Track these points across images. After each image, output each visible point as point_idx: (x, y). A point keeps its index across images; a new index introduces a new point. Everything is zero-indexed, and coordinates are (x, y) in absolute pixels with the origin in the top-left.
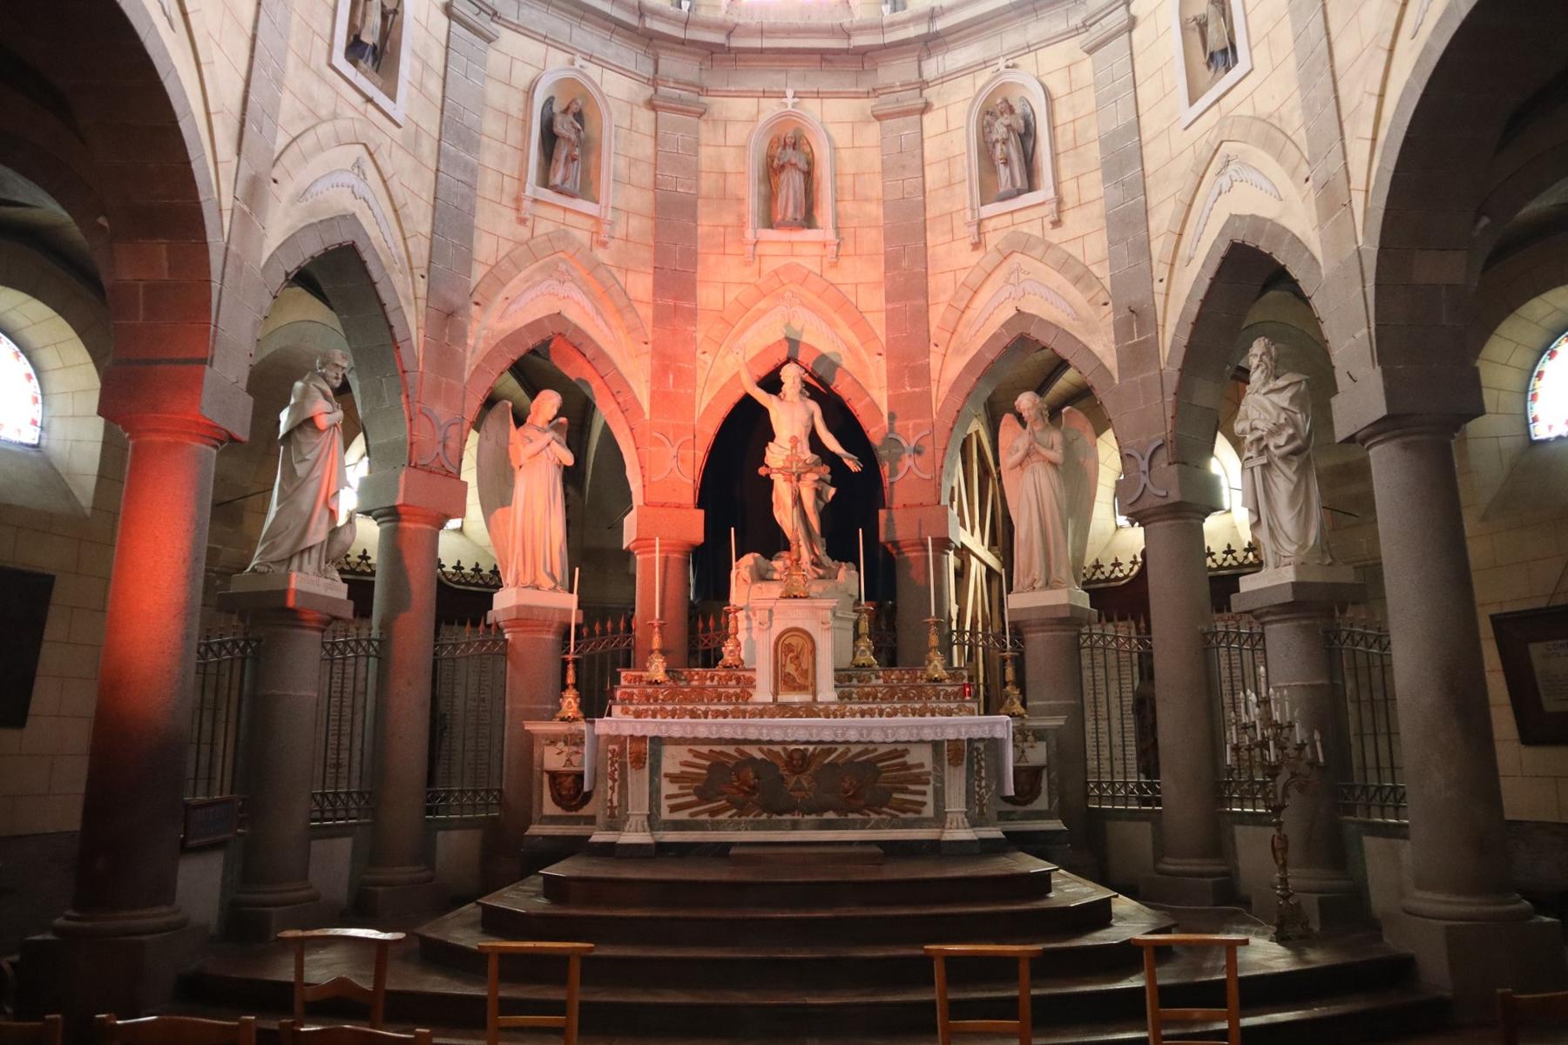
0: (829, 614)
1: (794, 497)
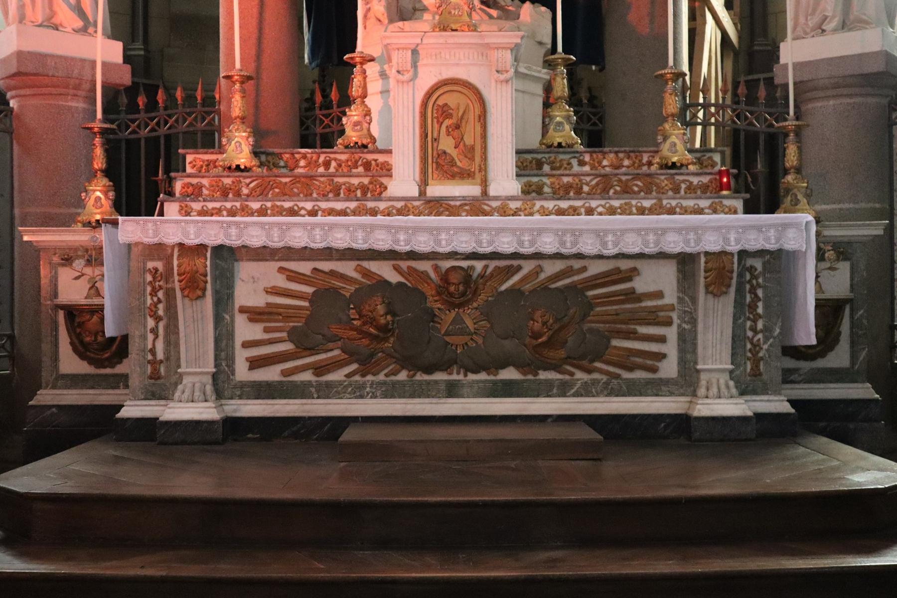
0: (508, 56)
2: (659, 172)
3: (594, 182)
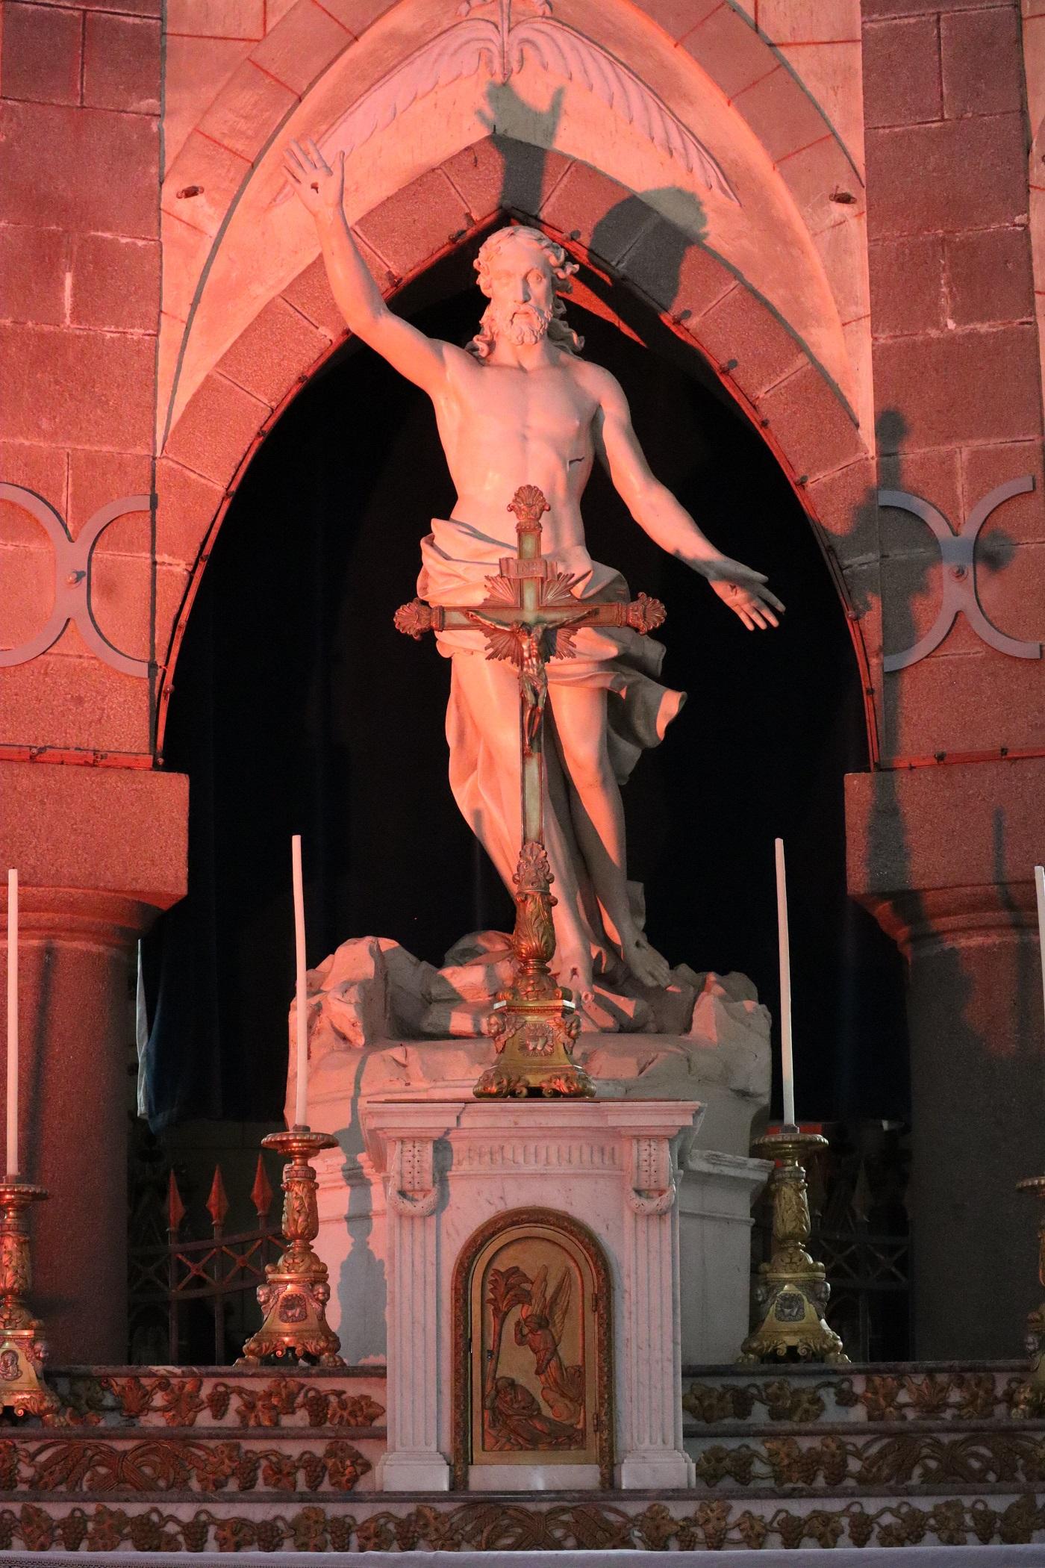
0: (664, 1156)
1: (522, 728)
2: (1028, 1423)
3: (874, 1449)
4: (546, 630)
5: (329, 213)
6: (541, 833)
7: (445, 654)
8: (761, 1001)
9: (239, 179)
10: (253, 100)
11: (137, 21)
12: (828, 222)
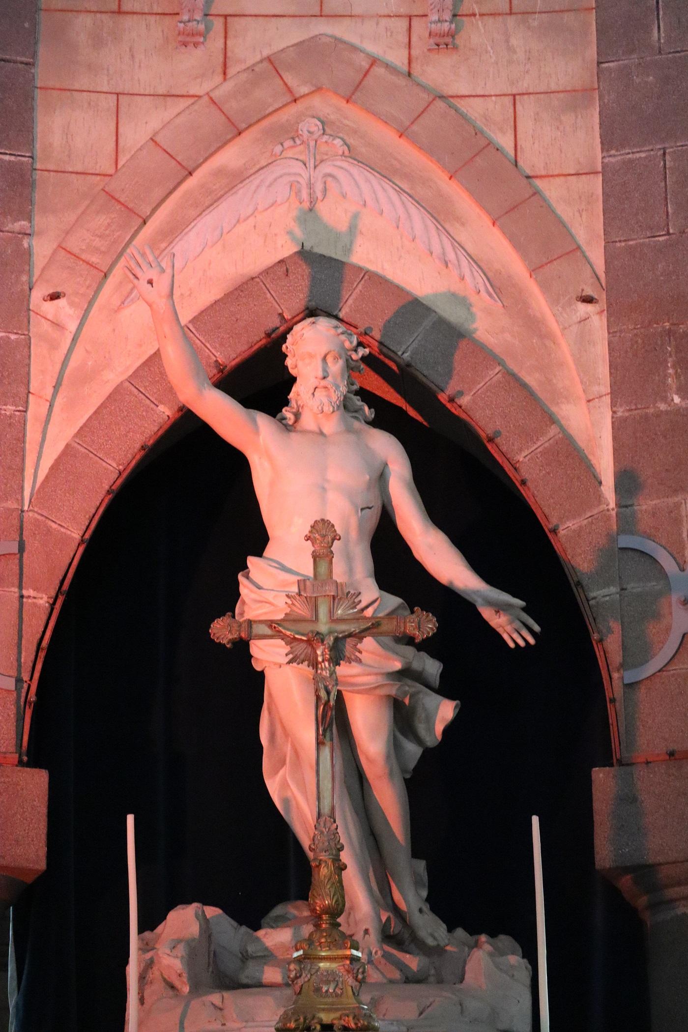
4: (337, 639)
5: (162, 304)
6: (333, 809)
7: (258, 668)
8: (523, 957)
9: (95, 286)
10: (106, 223)
11: (13, 158)
12: (575, 318)
